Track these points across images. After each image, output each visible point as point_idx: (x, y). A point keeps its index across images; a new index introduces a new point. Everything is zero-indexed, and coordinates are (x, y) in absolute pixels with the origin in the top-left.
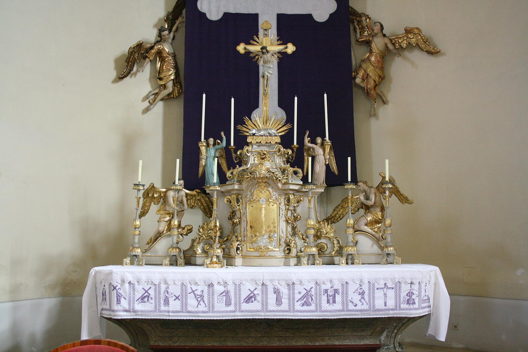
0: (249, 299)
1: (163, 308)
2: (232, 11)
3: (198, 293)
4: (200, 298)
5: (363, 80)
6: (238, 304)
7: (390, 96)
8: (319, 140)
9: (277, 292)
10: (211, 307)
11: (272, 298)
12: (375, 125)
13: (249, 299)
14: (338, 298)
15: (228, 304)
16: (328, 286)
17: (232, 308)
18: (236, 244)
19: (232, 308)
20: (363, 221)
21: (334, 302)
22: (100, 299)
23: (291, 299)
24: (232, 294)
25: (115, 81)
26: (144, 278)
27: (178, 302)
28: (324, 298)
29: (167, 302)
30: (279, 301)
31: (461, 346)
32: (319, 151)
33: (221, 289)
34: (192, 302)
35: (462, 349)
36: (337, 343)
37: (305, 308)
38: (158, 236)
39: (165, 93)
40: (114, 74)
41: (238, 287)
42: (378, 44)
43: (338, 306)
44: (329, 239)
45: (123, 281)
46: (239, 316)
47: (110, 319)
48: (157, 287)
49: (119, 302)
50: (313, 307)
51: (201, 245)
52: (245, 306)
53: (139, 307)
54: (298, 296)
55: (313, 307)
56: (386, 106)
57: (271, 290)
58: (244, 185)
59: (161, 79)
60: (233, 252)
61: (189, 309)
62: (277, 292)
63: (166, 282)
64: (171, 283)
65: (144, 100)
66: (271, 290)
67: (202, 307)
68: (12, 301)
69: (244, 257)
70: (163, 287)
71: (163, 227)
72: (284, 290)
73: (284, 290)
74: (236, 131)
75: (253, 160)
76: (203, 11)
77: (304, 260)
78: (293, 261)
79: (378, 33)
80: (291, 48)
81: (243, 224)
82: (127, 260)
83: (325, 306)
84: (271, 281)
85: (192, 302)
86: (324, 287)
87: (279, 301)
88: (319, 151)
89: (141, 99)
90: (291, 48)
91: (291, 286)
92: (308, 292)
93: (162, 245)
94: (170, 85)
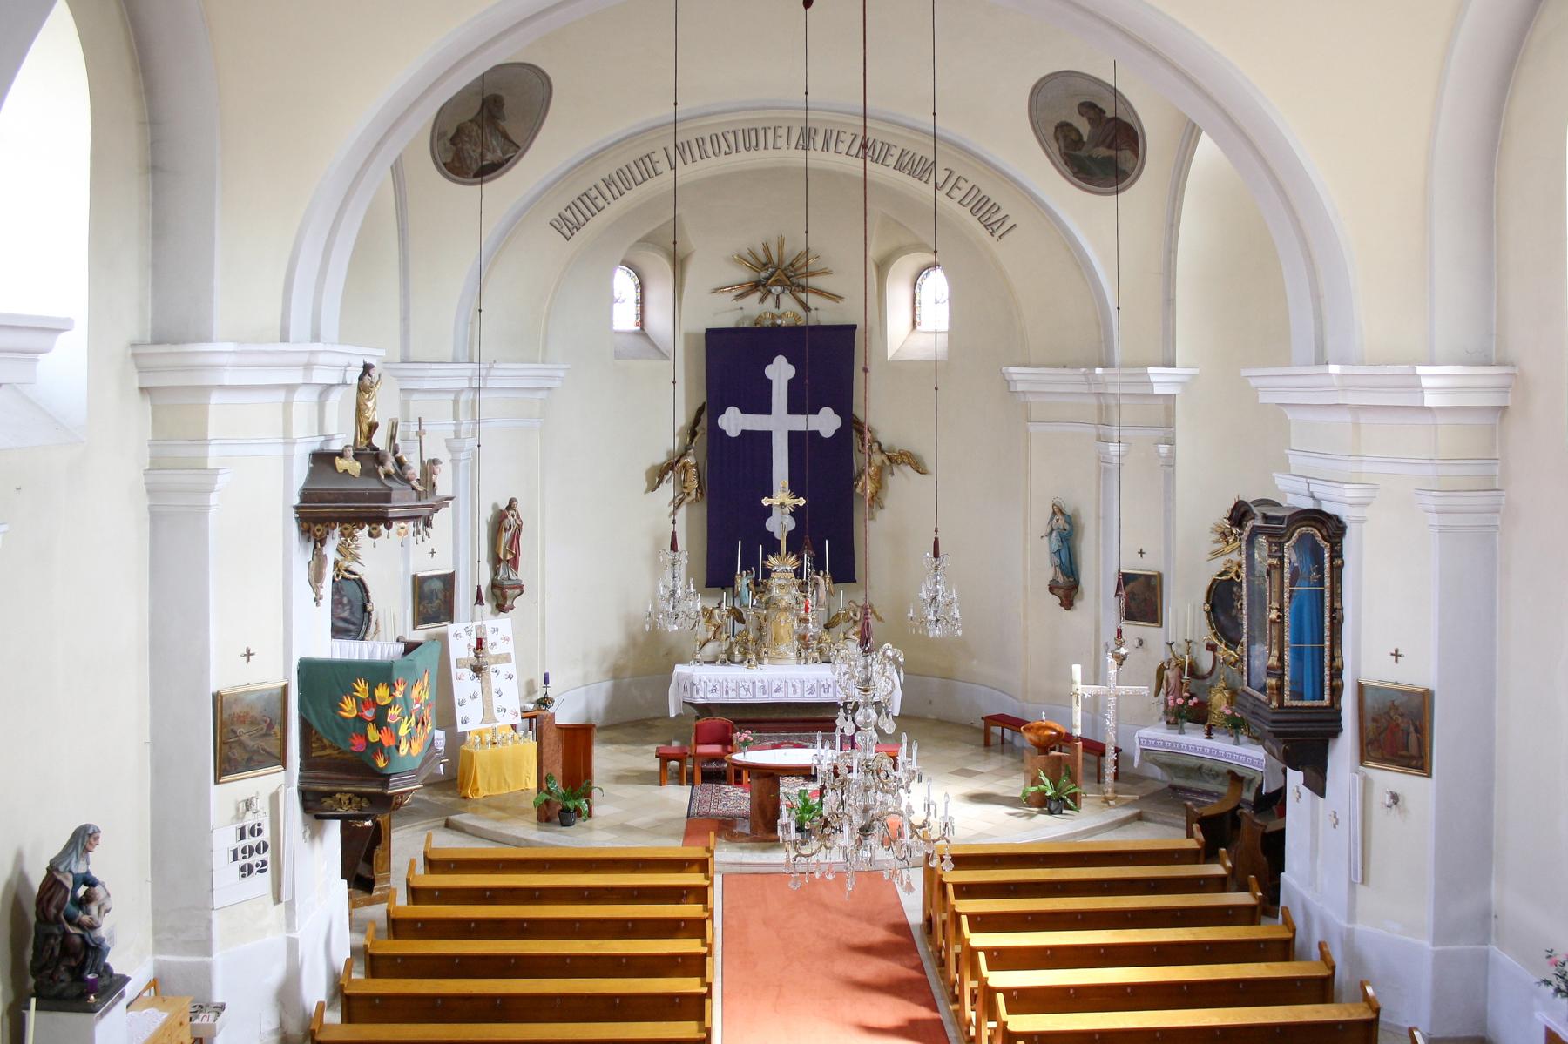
0: (777, 691)
1: (725, 696)
2: (749, 428)
3: (746, 687)
4: (747, 690)
5: (862, 491)
6: (770, 693)
7: (887, 502)
8: (822, 573)
9: (793, 686)
10: (754, 695)
11: (791, 689)
12: (871, 525)
13: (777, 691)
14: (831, 690)
15: (764, 694)
16: (824, 683)
17: (767, 696)
18: (764, 650)
19: (767, 696)
20: (851, 632)
21: (828, 691)
22: (682, 690)
23: (802, 691)
24: (767, 687)
25: (647, 492)
26: (713, 678)
27: (734, 692)
28: (822, 690)
29: (727, 693)
30: (795, 691)
31: (934, 717)
32: (821, 581)
33: (761, 684)
34: (742, 692)
35: (934, 719)
36: (818, 717)
37: (811, 696)
38: (708, 641)
39: (688, 499)
40: (645, 485)
41: (770, 684)
42: (877, 458)
43: (830, 695)
44: (828, 644)
45: (700, 681)
46: (770, 700)
47: (691, 704)
48: (721, 684)
49: (697, 692)
50: (815, 695)
51: (737, 648)
52: (775, 695)
53: (710, 696)
54: (806, 689)
55: (815, 695)
56: (882, 511)
57: (790, 684)
58: (770, 610)
59: (686, 488)
60: (762, 655)
61: (741, 696)
62: (793, 686)
63: (726, 680)
64: (729, 680)
65: (669, 506)
66: (790, 684)
67: (748, 696)
68: (586, 685)
69: (769, 658)
70: (725, 684)
71: (710, 635)
72: (798, 685)
73: (798, 685)
74: (763, 565)
75: (776, 592)
76: (723, 428)
77: (810, 661)
78: (803, 662)
79: (909, 335)
80: (802, 502)
81: (769, 636)
82: (692, 662)
83: (823, 694)
84: (791, 679)
85: (742, 692)
86: (822, 683)
87: (795, 691)
88: (821, 581)
89: (667, 504)
90: (802, 502)
91: (802, 682)
92: (812, 686)
93: (710, 649)
94: (694, 492)
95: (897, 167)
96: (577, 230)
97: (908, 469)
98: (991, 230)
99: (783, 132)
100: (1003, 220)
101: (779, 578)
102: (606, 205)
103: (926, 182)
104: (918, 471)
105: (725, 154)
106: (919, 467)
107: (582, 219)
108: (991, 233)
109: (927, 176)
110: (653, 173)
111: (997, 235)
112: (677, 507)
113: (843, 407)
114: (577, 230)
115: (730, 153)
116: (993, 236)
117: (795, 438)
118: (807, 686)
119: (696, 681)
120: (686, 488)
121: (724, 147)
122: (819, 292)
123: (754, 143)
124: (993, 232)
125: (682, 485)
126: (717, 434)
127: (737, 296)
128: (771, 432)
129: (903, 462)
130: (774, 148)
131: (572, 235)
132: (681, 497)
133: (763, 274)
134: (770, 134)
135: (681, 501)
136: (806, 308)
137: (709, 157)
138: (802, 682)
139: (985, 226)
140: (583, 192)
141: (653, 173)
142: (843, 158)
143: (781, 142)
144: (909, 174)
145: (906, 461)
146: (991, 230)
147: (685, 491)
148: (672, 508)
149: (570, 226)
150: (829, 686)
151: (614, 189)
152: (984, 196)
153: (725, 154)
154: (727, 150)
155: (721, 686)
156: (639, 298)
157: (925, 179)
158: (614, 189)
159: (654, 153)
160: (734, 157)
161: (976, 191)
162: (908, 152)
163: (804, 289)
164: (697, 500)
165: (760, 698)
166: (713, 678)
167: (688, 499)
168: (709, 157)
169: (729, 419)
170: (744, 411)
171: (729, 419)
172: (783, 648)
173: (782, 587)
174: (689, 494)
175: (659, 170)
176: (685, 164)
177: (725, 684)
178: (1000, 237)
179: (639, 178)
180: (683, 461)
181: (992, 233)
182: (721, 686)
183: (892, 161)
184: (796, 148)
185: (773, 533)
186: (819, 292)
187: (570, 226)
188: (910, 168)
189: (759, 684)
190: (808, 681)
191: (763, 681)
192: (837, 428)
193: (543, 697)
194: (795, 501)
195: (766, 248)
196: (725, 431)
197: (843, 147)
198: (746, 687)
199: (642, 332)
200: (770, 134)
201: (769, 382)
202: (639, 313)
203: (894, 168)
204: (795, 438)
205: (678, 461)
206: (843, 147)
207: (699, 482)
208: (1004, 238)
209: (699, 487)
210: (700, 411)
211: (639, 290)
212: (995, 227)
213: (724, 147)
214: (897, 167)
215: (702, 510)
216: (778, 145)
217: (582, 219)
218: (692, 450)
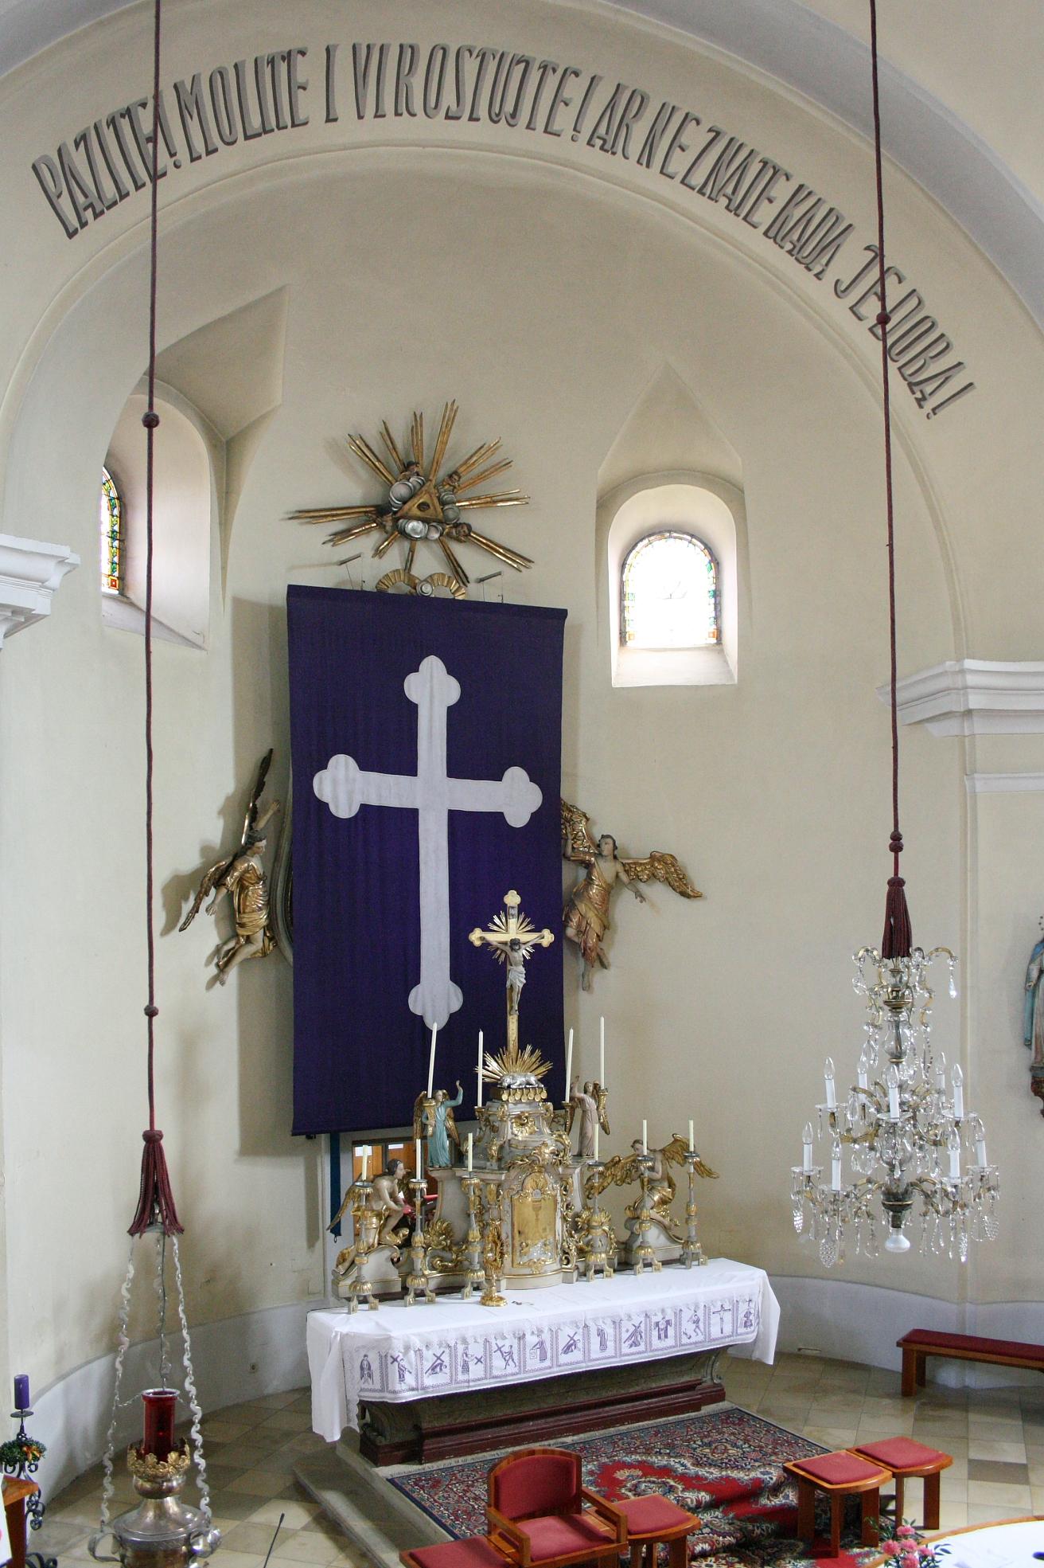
0: (568, 1349)
1: (461, 1377)
3: (506, 1349)
4: (508, 1356)
11: (595, 1341)
13: (568, 1349)
15: (543, 1359)
16: (659, 1318)
17: (547, 1363)
21: (666, 1337)
23: (618, 1341)
24: (548, 1346)
27: (480, 1366)
28: (655, 1333)
30: (603, 1346)
33: (535, 1339)
34: (498, 1362)
37: (634, 1349)
41: (555, 1334)
42: (605, 870)
43: (670, 1341)
45: (407, 1348)
46: (556, 1372)
49: (402, 1378)
50: (642, 1348)
52: (564, 1358)
53: (429, 1381)
54: (625, 1336)
57: (593, 1331)
59: (242, 925)
61: (495, 1373)
63: (465, 1341)
64: (470, 1340)
66: (593, 1331)
67: (511, 1369)
68: (62, 1377)
70: (461, 1348)
72: (609, 1331)
76: (325, 799)
83: (657, 1343)
84: (595, 1320)
85: (498, 1362)
86: (654, 1319)
89: (204, 961)
92: (637, 1328)
95: (772, 233)
96: (96, 216)
97: (658, 892)
98: (919, 395)
99: (575, 89)
100: (946, 375)
101: (516, 1103)
102: (171, 169)
103: (818, 276)
104: (684, 894)
105: (447, 117)
106: (684, 889)
107: (110, 191)
108: (919, 401)
109: (824, 261)
110: (287, 119)
111: (929, 405)
112: (222, 969)
113: (546, 774)
114: (96, 216)
115: (458, 118)
116: (921, 407)
117: (460, 823)
118: (628, 1327)
119: (398, 1352)
120: (242, 925)
121: (449, 99)
122: (491, 547)
123: (509, 107)
124: (924, 398)
125: (233, 919)
126: (313, 810)
127: (336, 534)
128: (416, 811)
129: (653, 876)
130: (546, 131)
131: (84, 225)
132: (231, 944)
133: (400, 490)
134: (552, 81)
135: (231, 956)
136: (459, 573)
137: (414, 115)
138: (617, 1324)
139: (910, 385)
140: (122, 106)
141: (287, 119)
142: (671, 190)
143: (564, 119)
144: (790, 252)
145: (661, 873)
146: (919, 395)
147: (241, 931)
148: (213, 970)
149: (81, 199)
150: (668, 1323)
151: (194, 125)
152: (927, 318)
153: (447, 117)
154: (454, 107)
155: (453, 1355)
156: (116, 528)
157: (817, 269)
158: (194, 125)
159: (303, 53)
160: (462, 129)
161: (914, 302)
162: (810, 193)
163: (462, 532)
164: (264, 954)
165: (536, 1369)
166: (435, 1340)
167: (247, 951)
168: (414, 115)
169: (335, 782)
170: (364, 766)
171: (335, 782)
172: (535, 1252)
173: (521, 1120)
174: (248, 939)
175: (301, 116)
176: (360, 117)
177: (461, 1348)
178: (934, 410)
179: (255, 122)
180: (241, 867)
181: (920, 402)
182: (453, 1355)
183: (766, 214)
184: (589, 143)
185: (421, 1017)
186: (491, 547)
187: (81, 199)
188: (795, 237)
189: (531, 1340)
190: (629, 1317)
191: (540, 1332)
192: (534, 809)
193: (13, 1438)
194: (532, 937)
195: (417, 420)
196: (327, 805)
197: (679, 163)
198: (506, 1349)
199: (121, 598)
200: (552, 81)
201: (413, 708)
202: (116, 559)
203: (766, 234)
204: (460, 823)
205: (230, 867)
206: (679, 163)
207: (270, 917)
208: (941, 413)
209: (270, 927)
210: (265, 764)
211: (116, 512)
212: (929, 389)
213: (449, 99)
214: (772, 233)
215: (274, 978)
216: (556, 126)
217: (110, 191)
218: (264, 842)
